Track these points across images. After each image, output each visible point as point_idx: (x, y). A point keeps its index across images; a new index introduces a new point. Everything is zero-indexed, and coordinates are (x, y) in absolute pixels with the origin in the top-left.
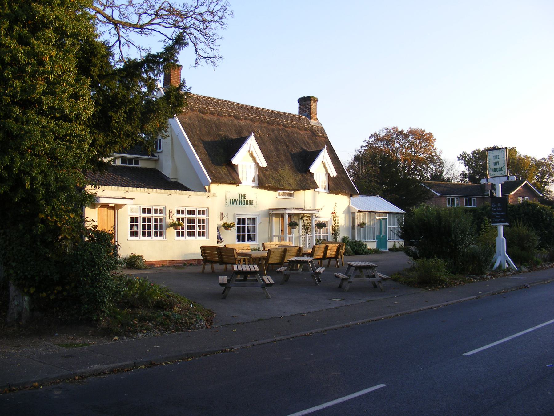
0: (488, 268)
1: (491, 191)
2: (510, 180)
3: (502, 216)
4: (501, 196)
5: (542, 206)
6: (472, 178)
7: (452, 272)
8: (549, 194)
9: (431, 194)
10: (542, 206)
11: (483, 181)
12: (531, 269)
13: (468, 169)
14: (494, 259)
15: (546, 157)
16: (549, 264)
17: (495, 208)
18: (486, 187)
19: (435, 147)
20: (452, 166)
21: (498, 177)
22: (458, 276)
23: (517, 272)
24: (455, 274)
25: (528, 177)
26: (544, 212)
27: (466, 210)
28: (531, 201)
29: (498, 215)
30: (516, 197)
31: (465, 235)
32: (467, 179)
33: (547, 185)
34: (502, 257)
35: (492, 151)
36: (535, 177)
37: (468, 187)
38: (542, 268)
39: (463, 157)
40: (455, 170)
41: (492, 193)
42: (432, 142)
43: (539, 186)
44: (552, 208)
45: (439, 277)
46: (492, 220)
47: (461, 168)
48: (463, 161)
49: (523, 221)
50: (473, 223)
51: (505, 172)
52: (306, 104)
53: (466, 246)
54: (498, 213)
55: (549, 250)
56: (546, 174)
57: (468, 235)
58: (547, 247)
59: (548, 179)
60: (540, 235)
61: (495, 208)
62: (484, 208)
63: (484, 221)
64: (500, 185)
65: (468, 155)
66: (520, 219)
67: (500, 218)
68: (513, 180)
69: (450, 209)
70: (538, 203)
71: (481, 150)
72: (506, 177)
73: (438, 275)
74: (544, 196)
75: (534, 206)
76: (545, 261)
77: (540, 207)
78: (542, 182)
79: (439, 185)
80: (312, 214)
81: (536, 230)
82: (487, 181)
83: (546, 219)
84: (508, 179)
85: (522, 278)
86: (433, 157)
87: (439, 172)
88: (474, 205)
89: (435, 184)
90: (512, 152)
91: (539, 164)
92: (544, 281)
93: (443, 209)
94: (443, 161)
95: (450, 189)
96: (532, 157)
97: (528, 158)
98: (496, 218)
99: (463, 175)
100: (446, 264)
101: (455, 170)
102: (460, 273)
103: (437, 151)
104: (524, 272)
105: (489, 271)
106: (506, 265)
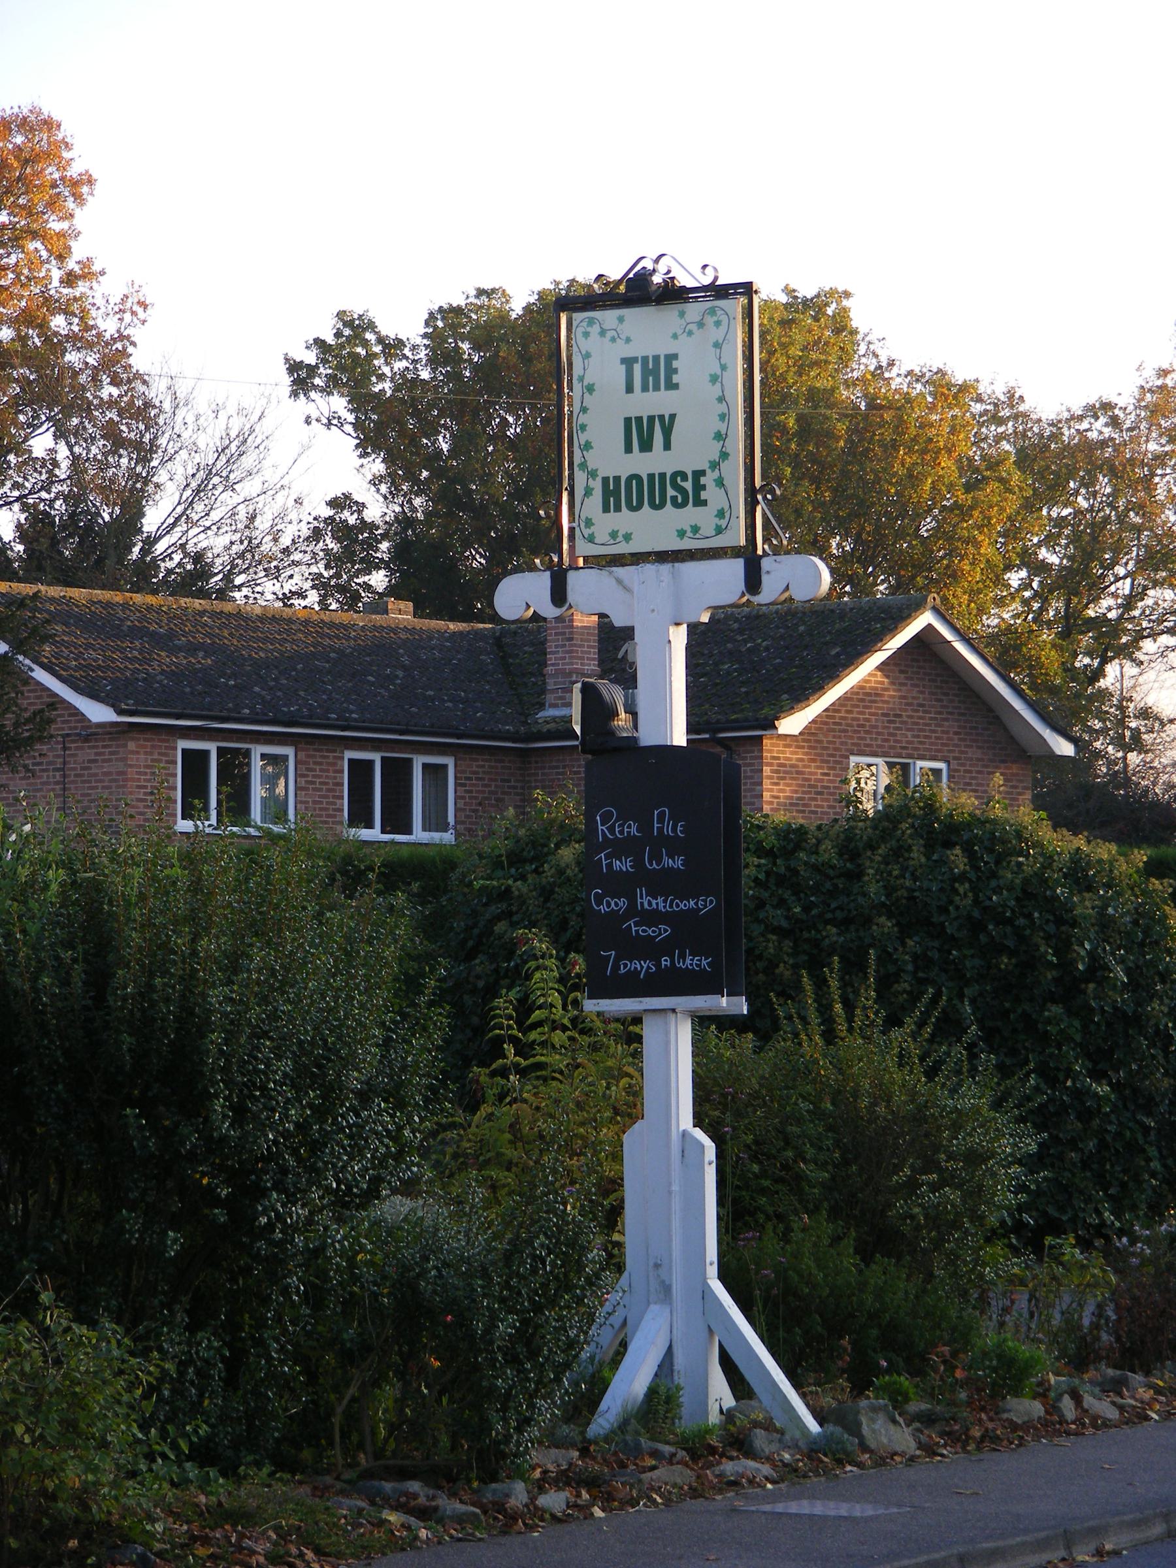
0: (547, 1411)
1: (589, 692)
2: (770, 592)
3: (688, 934)
4: (680, 738)
5: (1064, 843)
6: (430, 566)
7: (204, 1454)
8: (1136, 743)
9: (30, 703)
10: (1064, 843)
11: (520, 595)
12: (944, 1430)
13: (392, 478)
14: (603, 1336)
15: (1123, 393)
16: (1115, 1387)
17: (620, 848)
18: (555, 660)
19: (79, 250)
20: (234, 450)
21: (662, 557)
22: (258, 1487)
23: (822, 1460)
24: (230, 1471)
25: (954, 576)
26: (1085, 906)
27: (350, 871)
28: (968, 802)
29: (651, 918)
30: (824, 757)
31: (331, 1093)
32: (379, 579)
33: (1127, 652)
34: (678, 1313)
35: (609, 317)
36: (1015, 578)
37: (384, 647)
38: (1052, 1425)
39: (342, 362)
40: (272, 481)
41: (597, 710)
42: (53, 204)
43: (1051, 659)
44: (1155, 868)
45: (82, 1498)
46: (596, 965)
47: (319, 468)
48: (339, 403)
49: (884, 984)
50: (410, 984)
51: (727, 512)
52: (103, 273)
53: (347, 1202)
54: (645, 901)
55: (1113, 1257)
56: (1119, 549)
57: (364, 1097)
58: (1100, 1230)
59: (1129, 602)
60: (1042, 1118)
61: (620, 848)
62: (527, 854)
63: (519, 976)
64: (679, 638)
65: (393, 348)
66: (854, 965)
67: (666, 948)
68: (800, 594)
69: (194, 854)
70: (1026, 815)
71: (517, 308)
72: (737, 566)
73: (74, 1475)
74: (1087, 754)
75: (988, 844)
76: (1080, 1358)
77: (1049, 860)
78: (1072, 624)
79: (103, 624)
80: (713, 308)
81: (1004, 1071)
82: (559, 595)
83: (1097, 968)
84: (753, 581)
85: (858, 1510)
86: (55, 345)
87: (105, 490)
88: (435, 821)
89: (66, 614)
90: (813, 327)
91: (1051, 461)
92: (1069, 1540)
93: (133, 846)
94: (157, 391)
95: (212, 669)
96: (994, 386)
97: (947, 391)
98: (650, 949)
99: (343, 532)
100: (148, 1370)
101: (272, 481)
102: (285, 1464)
103: (103, 294)
104: (882, 1460)
105: (552, 1440)
106: (720, 1392)
